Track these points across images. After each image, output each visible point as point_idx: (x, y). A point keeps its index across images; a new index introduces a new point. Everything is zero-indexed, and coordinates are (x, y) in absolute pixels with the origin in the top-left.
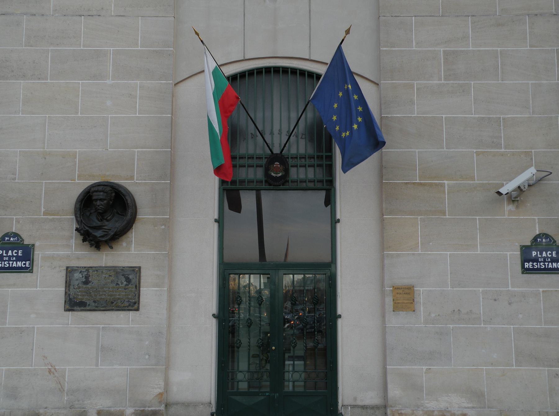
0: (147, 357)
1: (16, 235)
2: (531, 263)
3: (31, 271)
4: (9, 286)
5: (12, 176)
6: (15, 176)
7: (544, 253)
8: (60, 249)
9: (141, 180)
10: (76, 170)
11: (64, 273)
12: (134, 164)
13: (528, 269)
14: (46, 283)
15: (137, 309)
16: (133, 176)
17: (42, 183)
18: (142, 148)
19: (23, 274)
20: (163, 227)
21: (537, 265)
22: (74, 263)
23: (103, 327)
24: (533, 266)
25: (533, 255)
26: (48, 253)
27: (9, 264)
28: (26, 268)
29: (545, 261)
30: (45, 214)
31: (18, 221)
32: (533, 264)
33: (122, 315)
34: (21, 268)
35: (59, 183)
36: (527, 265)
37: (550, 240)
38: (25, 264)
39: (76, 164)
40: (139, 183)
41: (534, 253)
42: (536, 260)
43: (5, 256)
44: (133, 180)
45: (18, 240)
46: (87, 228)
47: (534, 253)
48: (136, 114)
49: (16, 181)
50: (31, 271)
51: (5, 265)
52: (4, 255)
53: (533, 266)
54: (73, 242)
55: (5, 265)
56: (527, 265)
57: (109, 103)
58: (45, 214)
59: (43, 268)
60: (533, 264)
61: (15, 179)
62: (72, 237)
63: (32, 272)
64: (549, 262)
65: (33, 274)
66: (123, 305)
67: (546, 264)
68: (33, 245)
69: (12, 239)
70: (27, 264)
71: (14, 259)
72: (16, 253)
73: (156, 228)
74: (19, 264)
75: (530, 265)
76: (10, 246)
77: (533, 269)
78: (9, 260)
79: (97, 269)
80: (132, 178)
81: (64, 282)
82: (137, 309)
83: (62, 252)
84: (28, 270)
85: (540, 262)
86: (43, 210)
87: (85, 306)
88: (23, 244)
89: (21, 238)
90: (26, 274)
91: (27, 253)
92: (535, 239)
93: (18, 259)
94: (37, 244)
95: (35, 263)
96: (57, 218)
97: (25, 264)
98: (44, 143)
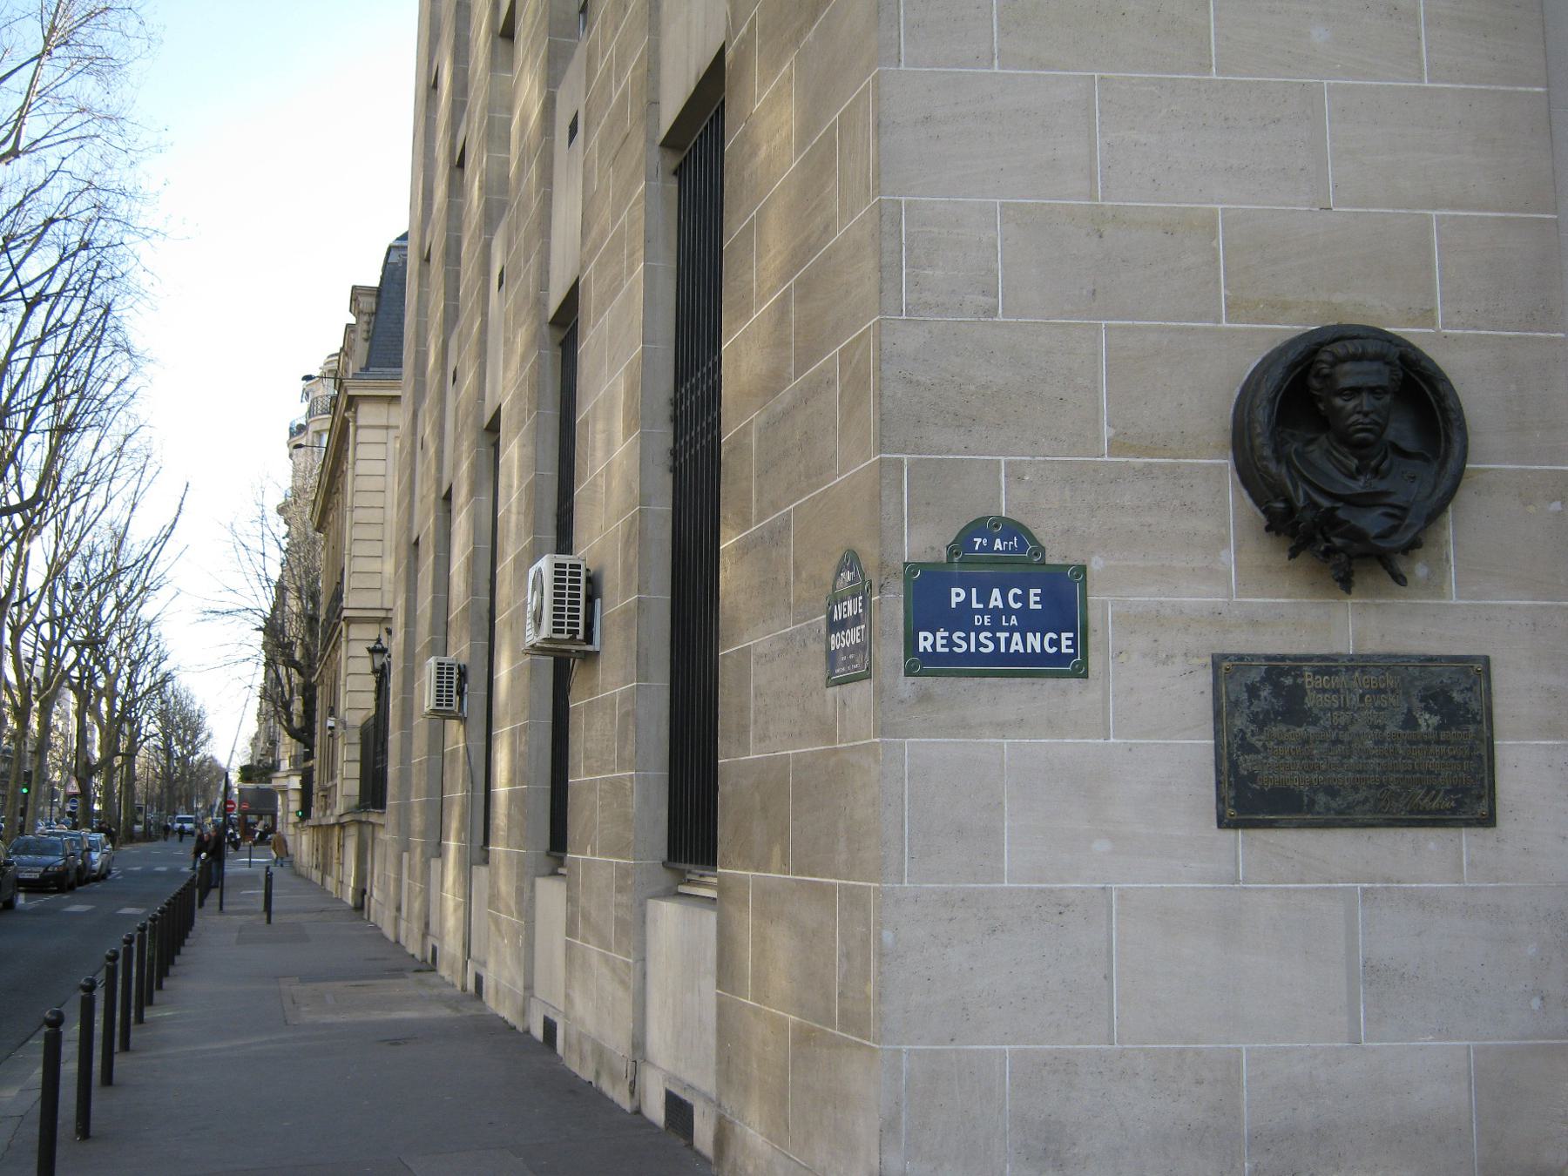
0: (1536, 1003)
1: (1012, 529)
2: (941, 633)
3: (1081, 672)
4: (1001, 728)
5: (981, 299)
6: (991, 300)
7: (996, 592)
8: (1188, 586)
9: (1463, 326)
10: (1217, 281)
11: (1205, 679)
12: (1429, 266)
13: (932, 658)
14: (1144, 721)
15: (1488, 820)
16: (1432, 311)
17: (1097, 328)
18: (1453, 206)
19: (1050, 682)
20: (1556, 506)
21: (967, 639)
22: (1242, 642)
23: (1365, 890)
24: (950, 643)
25: (954, 600)
26: (1145, 597)
27: (996, 641)
28: (1060, 659)
29: (995, 627)
30: (1116, 447)
31: (1015, 475)
32: (949, 639)
33: (1432, 845)
34: (1040, 658)
35: (1161, 330)
36: (925, 641)
37: (1020, 541)
38: (1053, 643)
39: (1216, 260)
40: (1456, 339)
41: (957, 596)
42: (961, 619)
43: (978, 611)
44: (1433, 324)
45: (1022, 546)
46: (1325, 503)
47: (957, 596)
48: (1421, 80)
49: (1000, 318)
50: (1081, 672)
51: (979, 644)
52: (975, 605)
53: (950, 643)
54: (1228, 557)
55: (979, 644)
56: (925, 641)
57: (1319, 35)
58: (1116, 447)
59: (1123, 657)
60: (949, 639)
61: (992, 312)
62: (1223, 541)
63: (1085, 676)
64: (1012, 630)
65: (1091, 681)
66: (1434, 805)
67: (1002, 636)
68: (1082, 569)
69: (998, 545)
70: (1064, 643)
71: (1014, 620)
72: (1016, 598)
73: (1531, 509)
74: (1034, 641)
75: (940, 642)
76: (1018, 569)
77: (951, 658)
78: (995, 627)
79: (1327, 665)
80: (1427, 317)
81: (1211, 714)
82: (1488, 820)
83: (1195, 597)
84: (1072, 665)
85: (978, 630)
86: (1107, 432)
87: (1299, 810)
88: (1042, 563)
89: (1033, 540)
90: (1063, 682)
91: (1063, 601)
92: (963, 542)
93: (1030, 621)
94: (1096, 565)
95: (1091, 640)
96: (1160, 466)
97: (1053, 643)
98: (1092, 177)
